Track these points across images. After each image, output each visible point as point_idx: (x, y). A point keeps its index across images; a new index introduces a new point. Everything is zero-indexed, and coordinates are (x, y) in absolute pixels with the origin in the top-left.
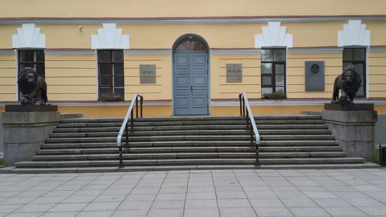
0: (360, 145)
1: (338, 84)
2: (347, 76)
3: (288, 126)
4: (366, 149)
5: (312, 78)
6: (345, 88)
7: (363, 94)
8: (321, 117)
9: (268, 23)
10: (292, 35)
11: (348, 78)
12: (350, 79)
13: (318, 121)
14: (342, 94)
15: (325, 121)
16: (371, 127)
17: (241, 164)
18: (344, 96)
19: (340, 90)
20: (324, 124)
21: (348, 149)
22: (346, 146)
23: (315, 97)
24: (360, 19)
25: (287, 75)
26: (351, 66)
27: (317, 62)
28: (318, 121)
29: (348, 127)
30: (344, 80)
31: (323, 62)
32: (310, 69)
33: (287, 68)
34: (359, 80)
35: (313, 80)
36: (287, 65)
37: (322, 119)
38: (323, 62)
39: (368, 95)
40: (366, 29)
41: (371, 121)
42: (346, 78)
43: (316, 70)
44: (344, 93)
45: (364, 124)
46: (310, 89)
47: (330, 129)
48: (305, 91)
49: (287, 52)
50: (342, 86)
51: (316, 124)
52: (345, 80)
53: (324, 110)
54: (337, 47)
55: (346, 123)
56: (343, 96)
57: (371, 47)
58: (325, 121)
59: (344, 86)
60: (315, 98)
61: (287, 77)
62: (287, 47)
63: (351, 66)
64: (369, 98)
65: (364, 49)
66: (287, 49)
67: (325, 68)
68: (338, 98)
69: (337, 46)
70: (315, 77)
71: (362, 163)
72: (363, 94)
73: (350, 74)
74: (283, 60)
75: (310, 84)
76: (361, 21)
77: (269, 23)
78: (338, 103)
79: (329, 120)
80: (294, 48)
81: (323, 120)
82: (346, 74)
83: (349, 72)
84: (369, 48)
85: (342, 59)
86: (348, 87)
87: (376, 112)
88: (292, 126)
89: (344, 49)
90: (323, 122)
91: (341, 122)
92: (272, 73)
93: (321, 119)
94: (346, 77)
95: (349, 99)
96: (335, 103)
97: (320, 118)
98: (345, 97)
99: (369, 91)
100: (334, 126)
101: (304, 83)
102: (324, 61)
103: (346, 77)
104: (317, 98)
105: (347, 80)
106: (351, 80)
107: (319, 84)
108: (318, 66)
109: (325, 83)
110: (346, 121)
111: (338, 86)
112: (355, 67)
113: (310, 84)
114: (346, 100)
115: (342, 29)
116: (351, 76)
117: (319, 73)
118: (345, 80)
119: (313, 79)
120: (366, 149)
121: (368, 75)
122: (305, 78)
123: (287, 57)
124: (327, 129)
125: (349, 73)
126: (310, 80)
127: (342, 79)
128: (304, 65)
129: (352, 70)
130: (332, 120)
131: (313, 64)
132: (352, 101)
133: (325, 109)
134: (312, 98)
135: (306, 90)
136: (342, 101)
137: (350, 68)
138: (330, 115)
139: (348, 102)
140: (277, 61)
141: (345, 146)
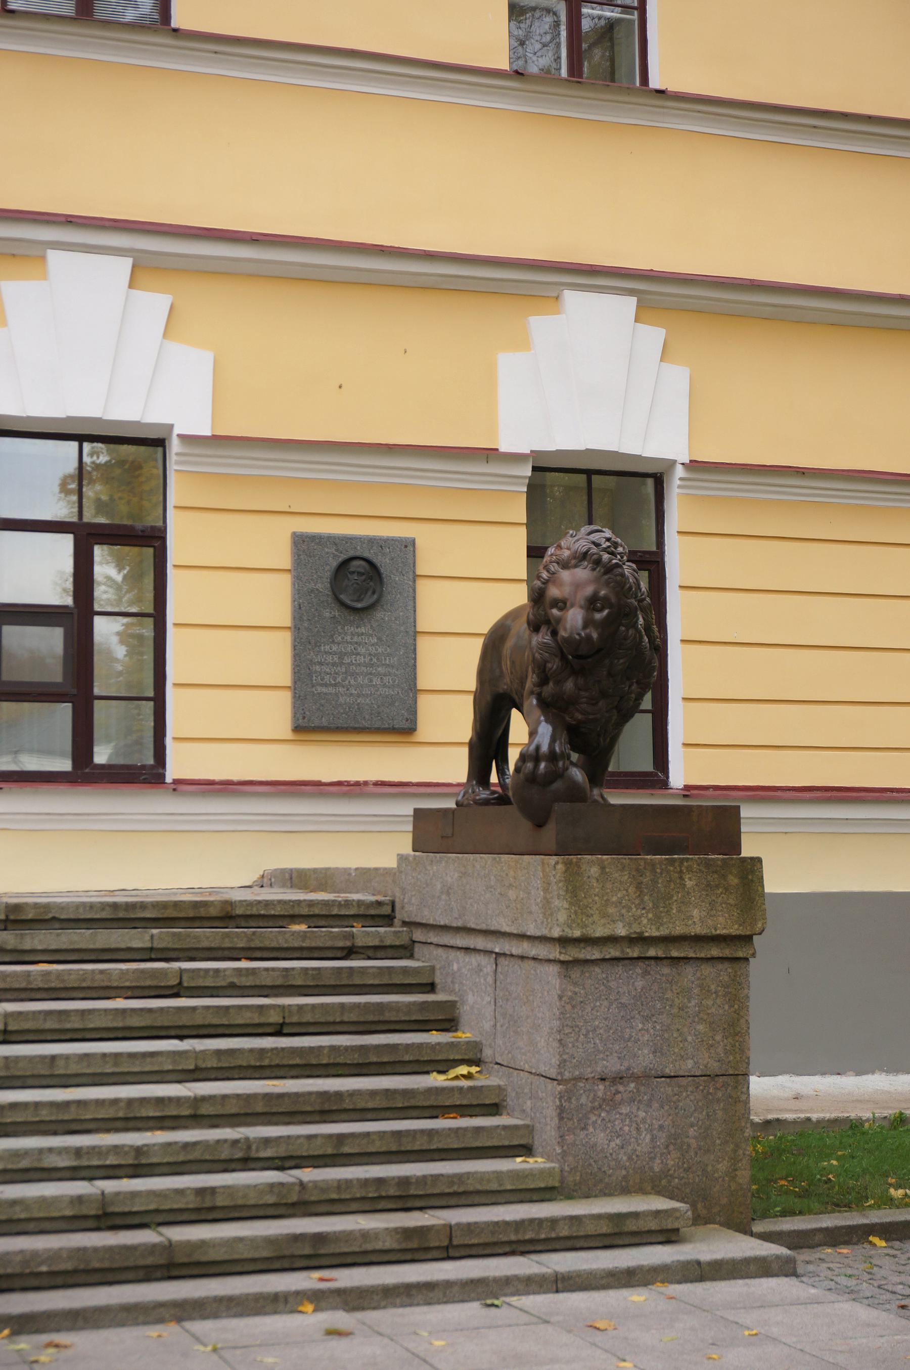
0: (649, 1105)
1: (506, 665)
2: (562, 604)
3: (154, 973)
4: (692, 1132)
5: (335, 648)
6: (549, 688)
7: (646, 764)
8: (393, 904)
9: (43, 258)
10: (208, 357)
11: (574, 618)
12: (587, 623)
13: (363, 934)
14: (532, 734)
15: (418, 935)
16: (724, 972)
17: (119, 1124)
18: (545, 748)
19: (516, 716)
20: (411, 957)
21: (570, 1138)
22: (561, 1112)
23: (361, 778)
24: (631, 292)
25: (172, 615)
26: (595, 537)
27: (372, 541)
28: (363, 934)
29: (575, 973)
30: (543, 637)
31: (409, 545)
32: (323, 586)
33: (170, 571)
34: (646, 639)
35: (347, 660)
36: (175, 554)
37: (396, 921)
38: (409, 545)
39: (678, 777)
40: (665, 355)
41: (735, 930)
42: (559, 620)
43: (361, 593)
44: (545, 730)
45: (675, 954)
46: (324, 721)
47: (452, 991)
48: (289, 735)
49: (172, 459)
50: (531, 680)
51: (350, 952)
52: (554, 633)
53: (413, 853)
54: (490, 454)
55: (563, 941)
56: (538, 748)
57: (694, 466)
58: (418, 935)
59: (544, 680)
60: (357, 784)
61: (172, 635)
62: (177, 431)
63: (595, 537)
64: (687, 788)
65: (650, 482)
66: (175, 446)
67: (421, 585)
68: (501, 772)
69: (497, 450)
70: (356, 639)
71: (670, 1237)
72: (646, 764)
73: (589, 590)
74: (152, 520)
75: (324, 690)
76: (632, 301)
77: (53, 256)
78: (502, 800)
79: (445, 928)
80: (216, 440)
81: (405, 923)
82: (554, 592)
83: (583, 573)
84: (680, 472)
85: (523, 531)
86: (569, 685)
87: (756, 862)
88: (182, 971)
89: (535, 469)
90: (404, 940)
91: (523, 937)
92: (69, 601)
93: (388, 919)
94: (555, 611)
95: (578, 774)
96: (486, 802)
97: (386, 910)
98: (552, 757)
99: (685, 745)
100: (228, 913)
101: (287, 680)
102: (413, 542)
103: (561, 609)
104: (366, 783)
105: (563, 633)
106: (595, 635)
107: (384, 686)
108: (373, 572)
109: (421, 684)
110: (556, 933)
111: (504, 686)
112: (616, 545)
113: (324, 690)
114: (555, 775)
115: (522, 343)
116: (592, 603)
117: (379, 614)
118: (554, 633)
119: (341, 655)
120: (692, 1132)
121: (680, 645)
122: (294, 647)
123: (172, 499)
124: (431, 987)
125: (577, 586)
126: (329, 659)
127: (535, 627)
128: (285, 560)
129: (598, 562)
130: (459, 924)
131: (343, 557)
132: (596, 792)
133: (414, 851)
134: (339, 783)
135: (298, 729)
136: (532, 779)
137: (582, 545)
138: (448, 890)
139: (575, 794)
140: (102, 520)
141: (550, 1111)
